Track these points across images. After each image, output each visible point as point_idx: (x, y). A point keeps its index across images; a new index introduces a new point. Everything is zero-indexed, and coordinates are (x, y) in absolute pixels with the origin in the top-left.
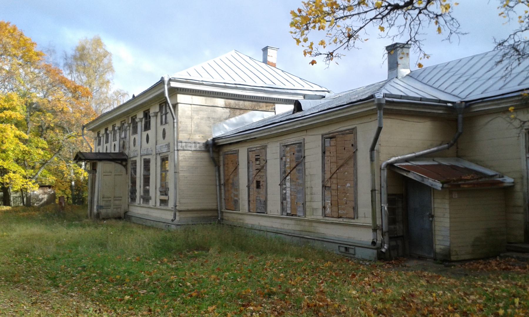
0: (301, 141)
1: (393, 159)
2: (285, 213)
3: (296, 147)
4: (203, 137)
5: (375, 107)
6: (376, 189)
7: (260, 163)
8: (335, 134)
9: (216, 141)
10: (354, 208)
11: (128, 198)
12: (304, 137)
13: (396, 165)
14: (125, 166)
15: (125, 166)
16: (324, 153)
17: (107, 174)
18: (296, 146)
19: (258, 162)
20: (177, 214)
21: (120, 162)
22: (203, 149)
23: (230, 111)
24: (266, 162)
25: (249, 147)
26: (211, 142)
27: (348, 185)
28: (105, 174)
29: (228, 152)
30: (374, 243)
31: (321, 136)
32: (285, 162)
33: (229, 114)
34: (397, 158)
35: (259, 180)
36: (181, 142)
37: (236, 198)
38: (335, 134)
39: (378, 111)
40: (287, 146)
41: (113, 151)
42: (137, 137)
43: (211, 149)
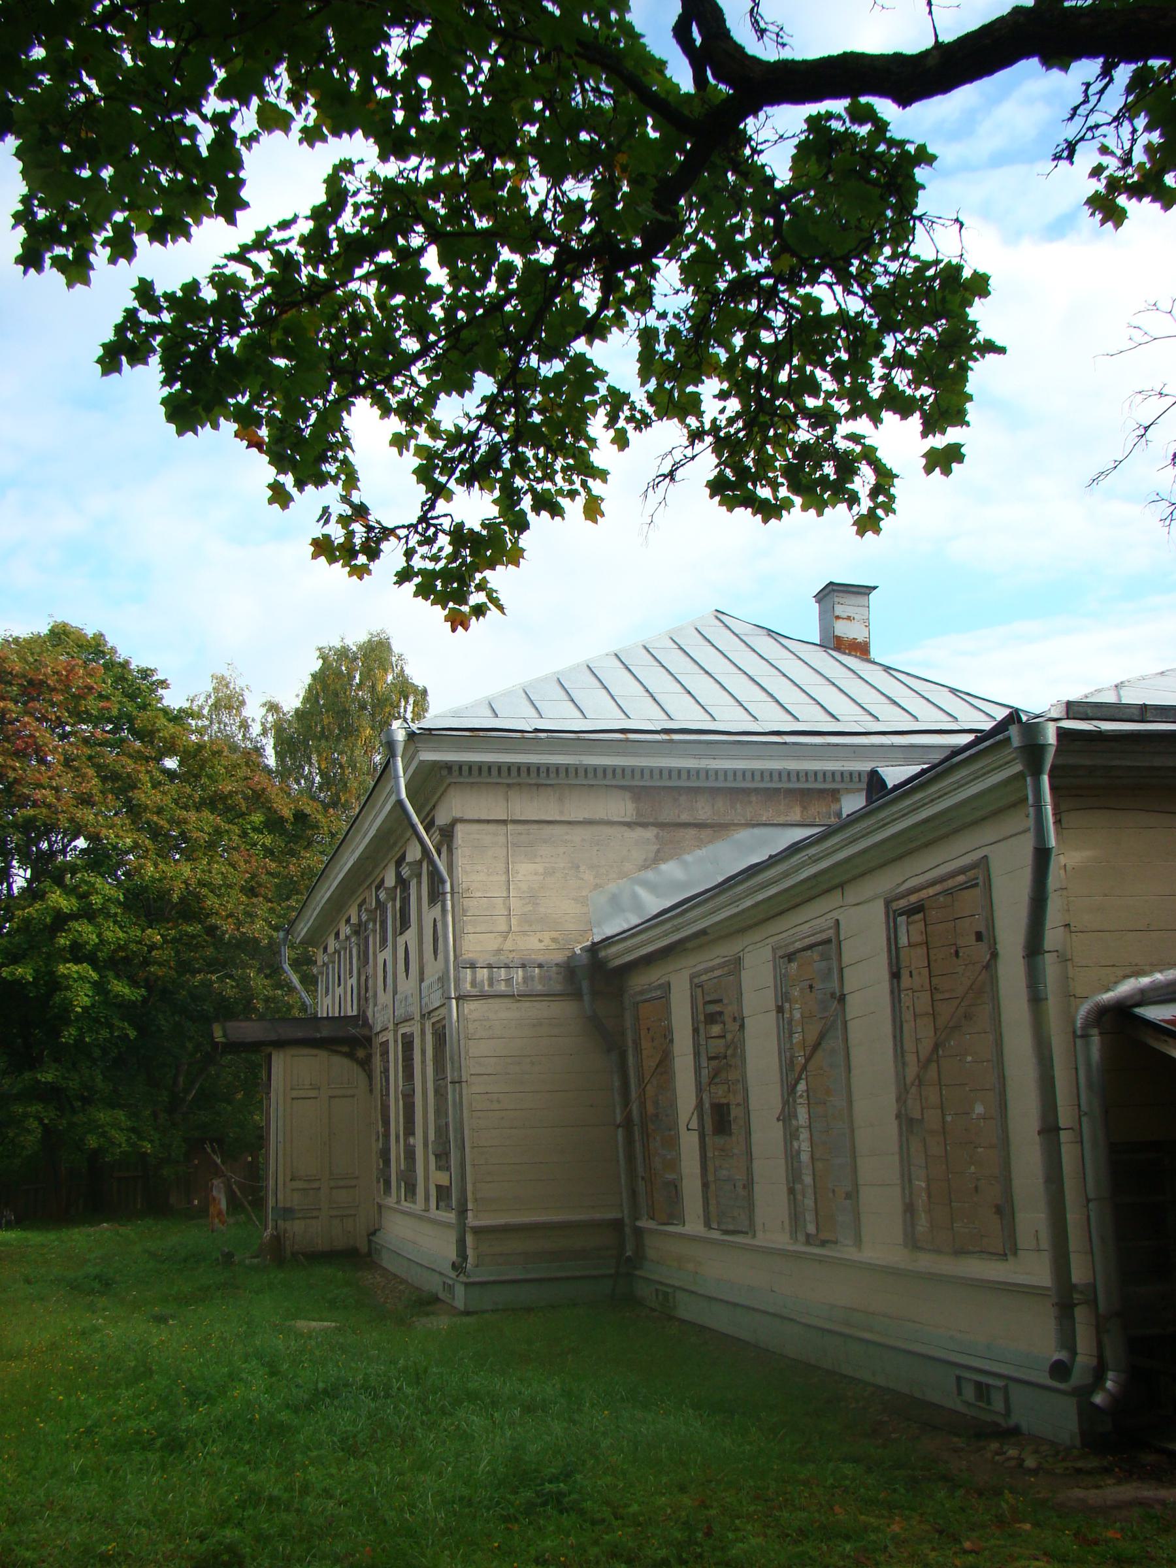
0: (831, 933)
1: (1126, 988)
2: (802, 1238)
3: (816, 957)
4: (554, 940)
5: (1018, 768)
6: (1061, 1125)
7: (725, 1031)
8: (923, 894)
9: (602, 954)
10: (999, 1210)
11: (378, 1182)
12: (835, 915)
13: (1140, 1011)
14: (365, 1064)
15: (365, 1064)
16: (895, 975)
17: (302, 1094)
18: (815, 955)
19: (716, 1030)
20: (469, 1239)
21: (345, 1049)
22: (558, 988)
23: (657, 837)
24: (742, 1026)
25: (694, 970)
26: (585, 959)
27: (979, 1109)
28: (295, 1094)
29: (642, 993)
30: (1060, 1370)
31: (879, 906)
32: (791, 1020)
33: (656, 847)
34: (1145, 981)
35: (724, 1101)
36: (473, 967)
37: (671, 1176)
38: (923, 894)
39: (1029, 779)
40: (790, 957)
41: (350, 1013)
42: (387, 954)
43: (585, 985)
